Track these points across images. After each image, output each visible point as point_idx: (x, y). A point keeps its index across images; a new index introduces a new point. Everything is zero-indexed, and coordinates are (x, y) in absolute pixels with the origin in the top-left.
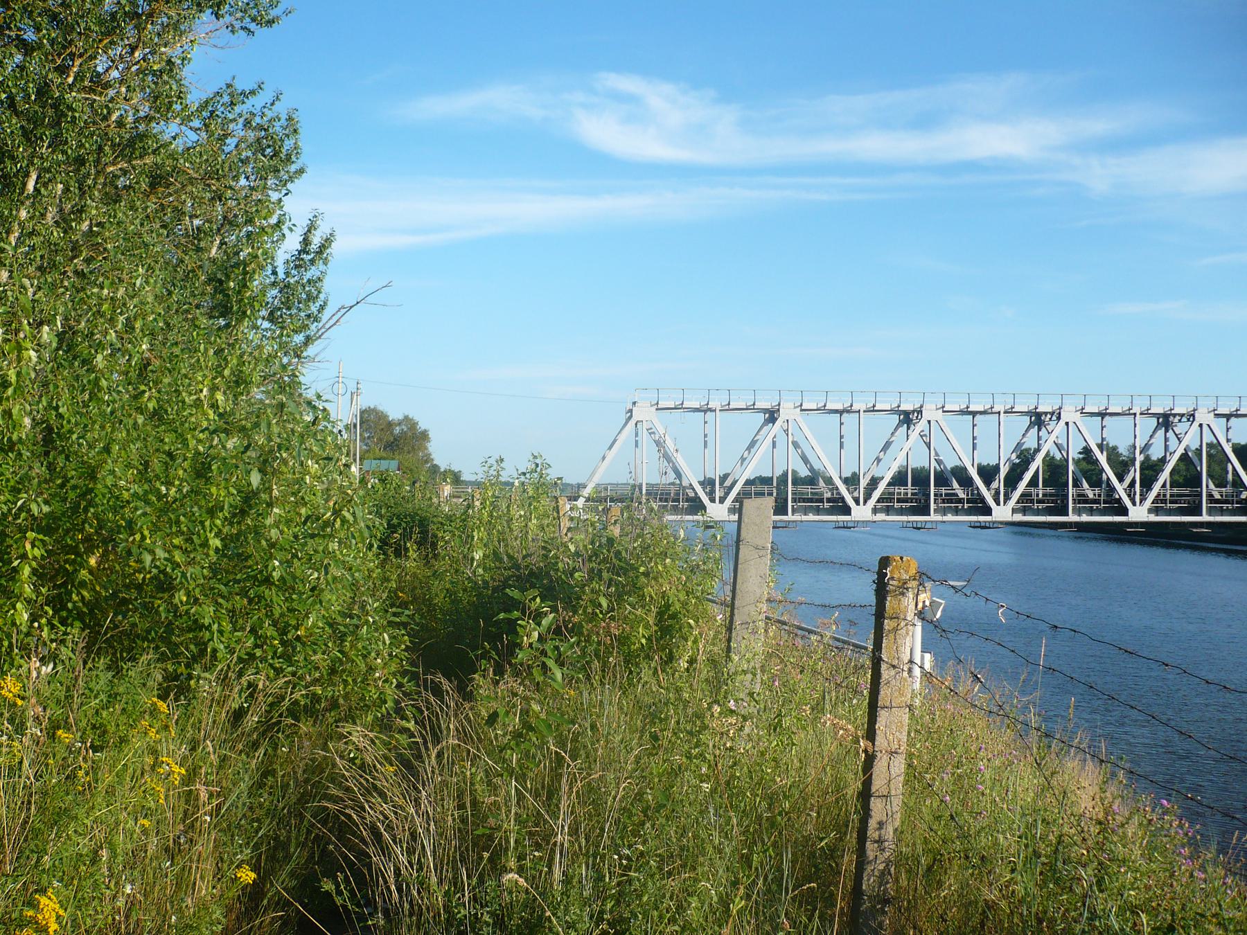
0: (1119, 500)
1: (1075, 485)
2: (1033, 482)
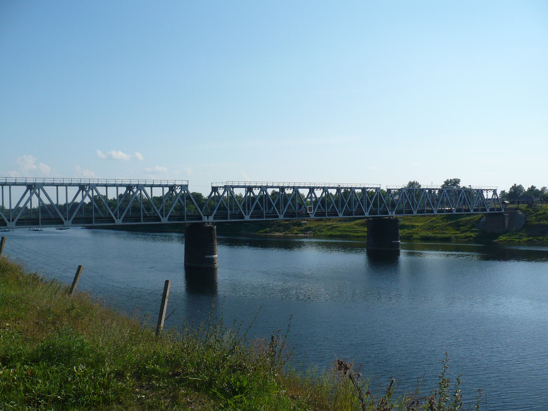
0: (158, 216)
1: (143, 211)
2: (128, 211)
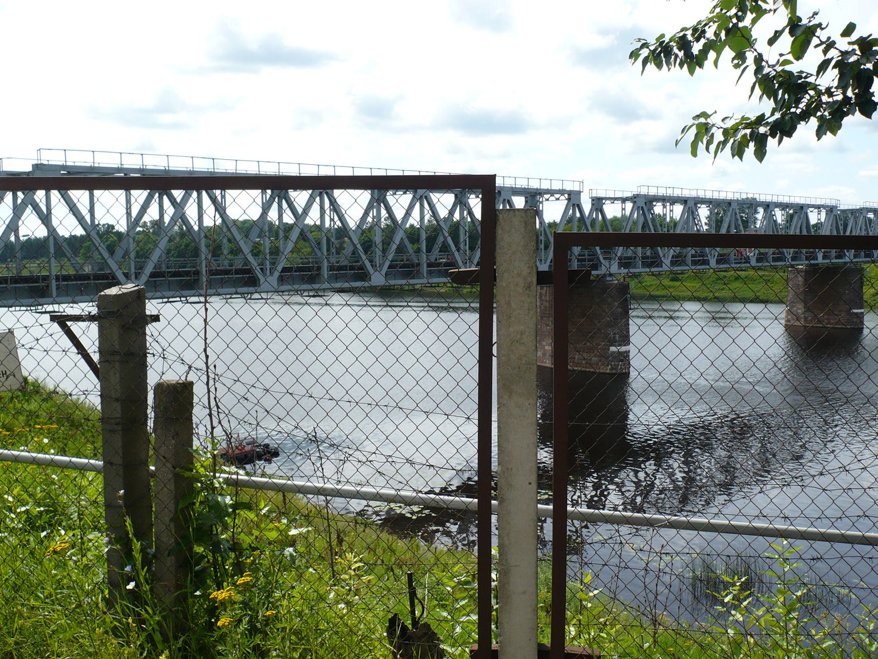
0: (362, 267)
